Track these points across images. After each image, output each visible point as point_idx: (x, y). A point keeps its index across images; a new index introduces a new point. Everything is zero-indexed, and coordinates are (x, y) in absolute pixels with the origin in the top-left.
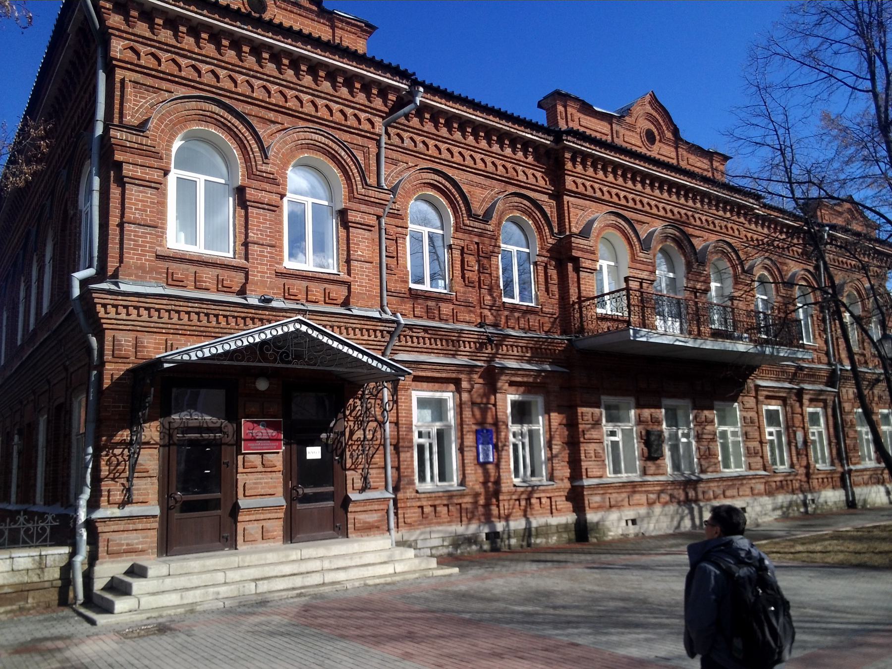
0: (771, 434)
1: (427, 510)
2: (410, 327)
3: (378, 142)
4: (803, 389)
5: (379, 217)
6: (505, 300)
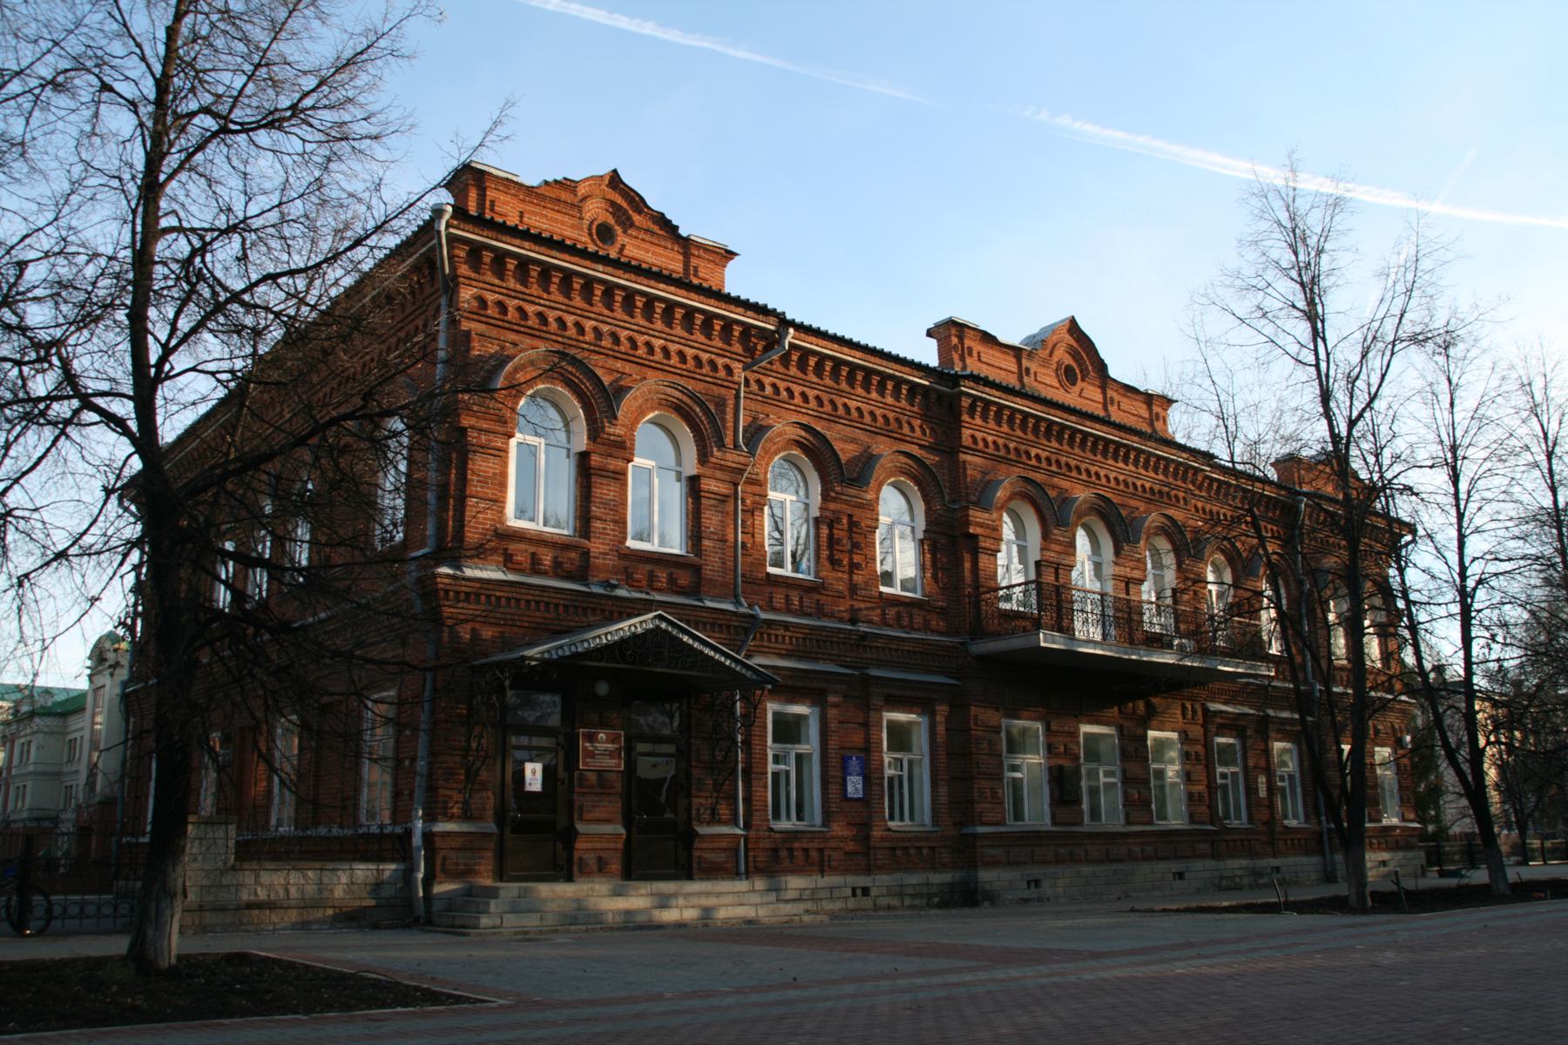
0: (1224, 776)
1: (814, 854)
2: (769, 623)
3: (738, 391)
6: (883, 589)
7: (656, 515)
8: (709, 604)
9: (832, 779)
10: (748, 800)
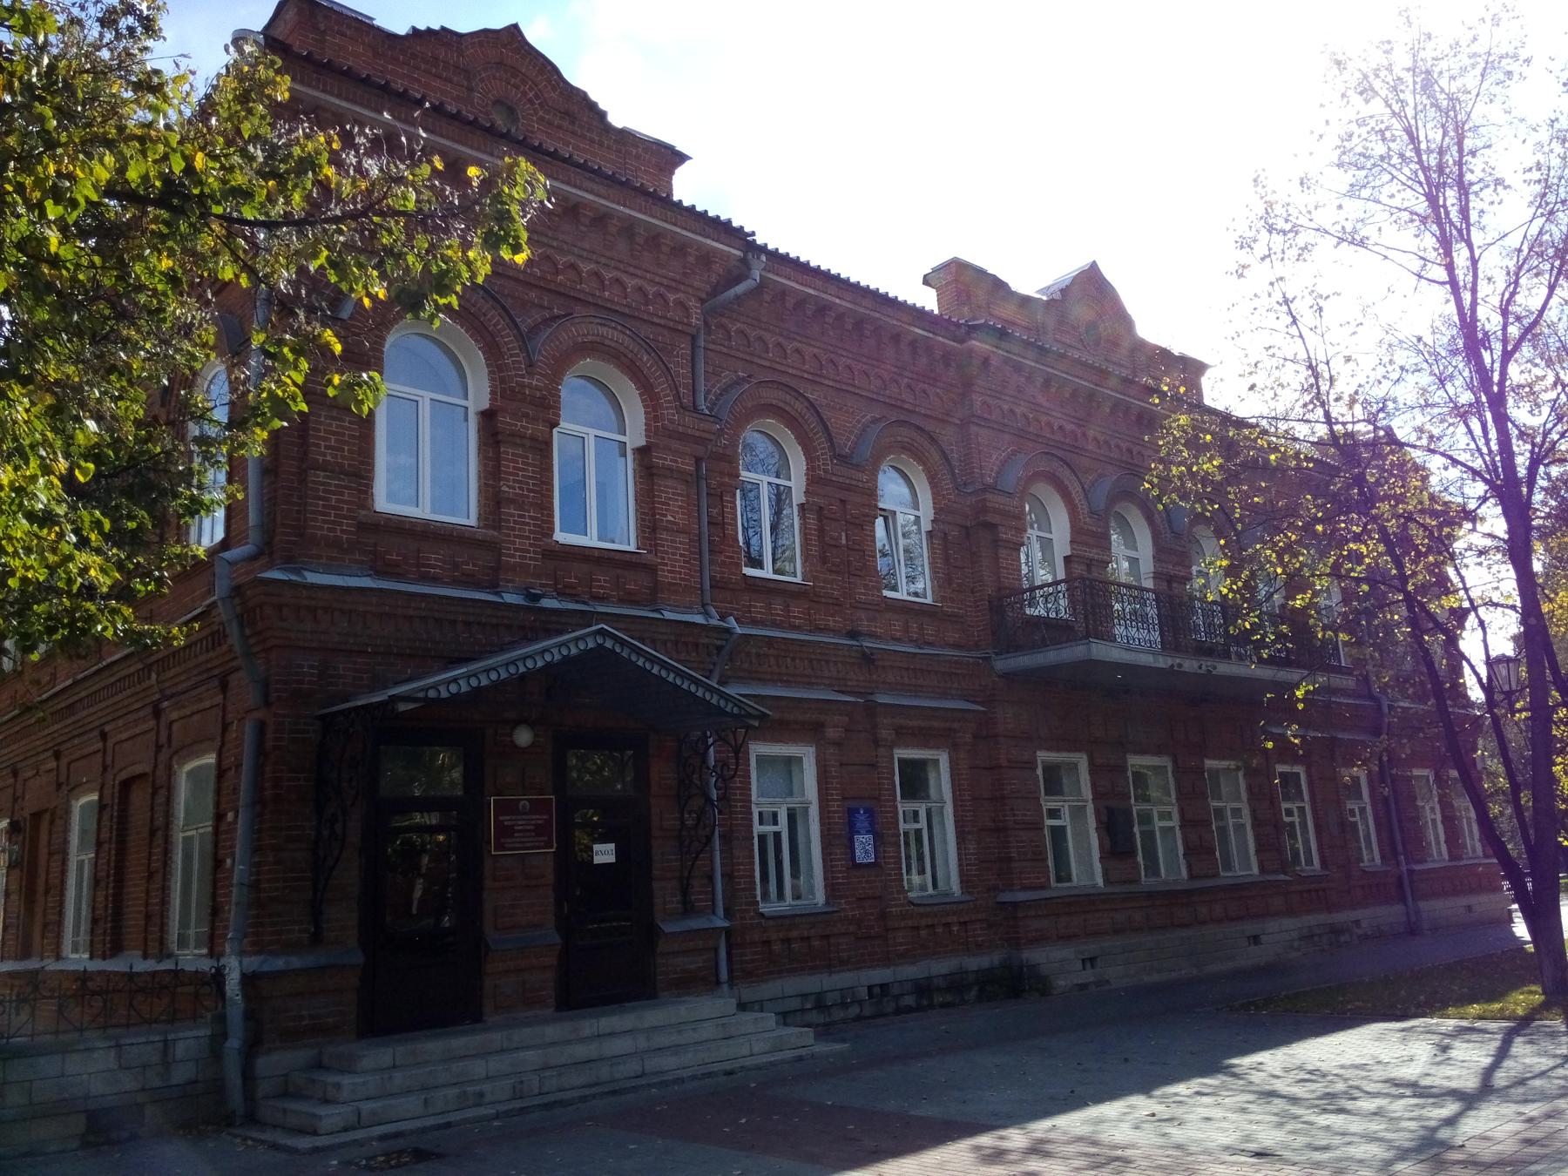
4: (1334, 739)
5: (698, 460)
7: (598, 510)
8: (668, 615)
9: (837, 839)
10: (728, 877)
